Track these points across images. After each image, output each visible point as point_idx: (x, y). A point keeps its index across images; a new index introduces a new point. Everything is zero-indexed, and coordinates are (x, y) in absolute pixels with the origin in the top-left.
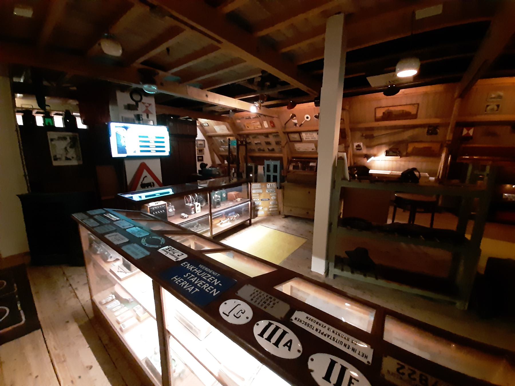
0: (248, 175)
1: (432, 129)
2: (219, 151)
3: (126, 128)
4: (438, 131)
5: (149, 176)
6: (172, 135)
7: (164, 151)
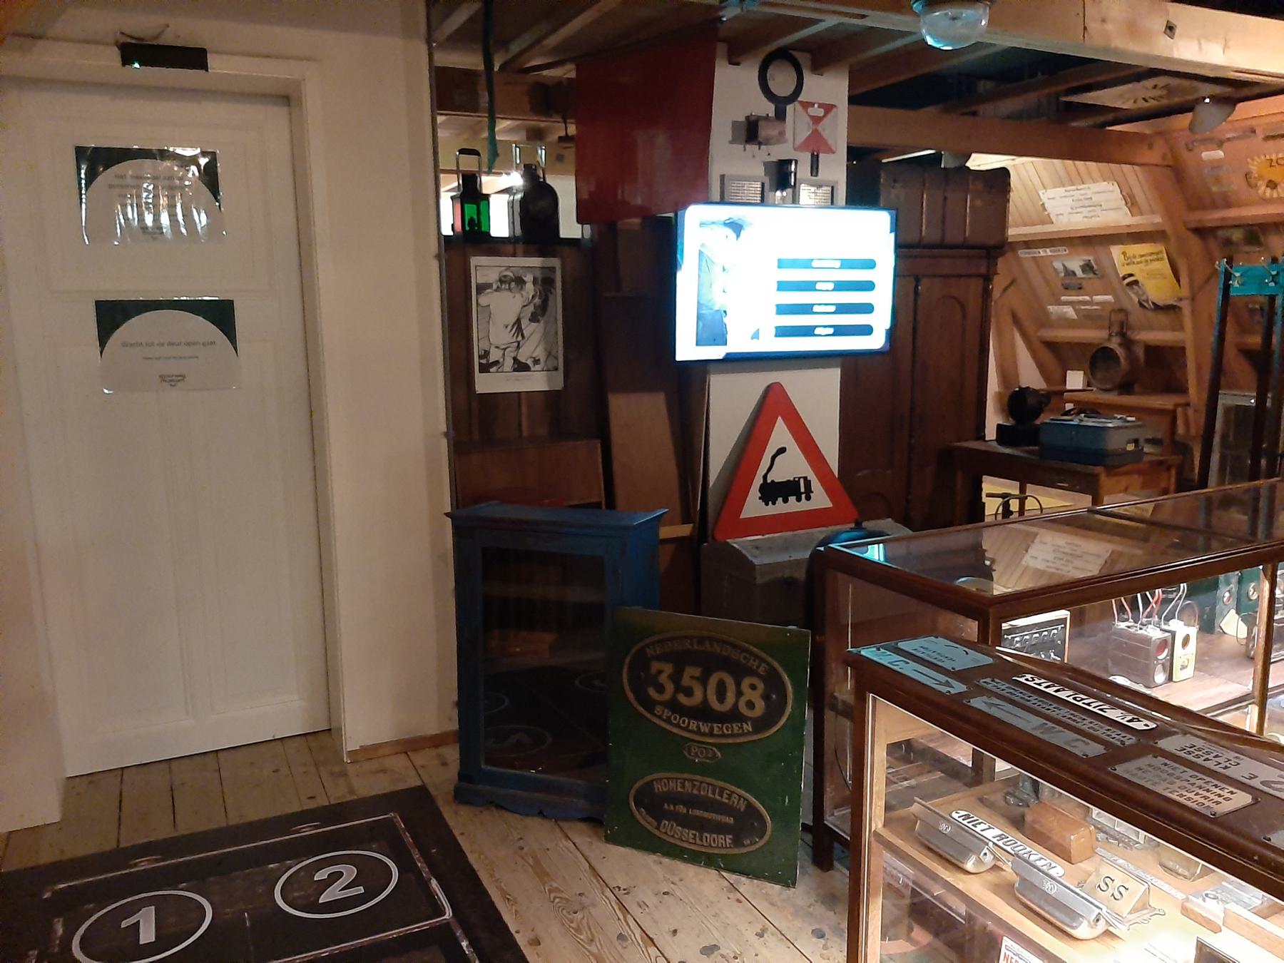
0: (1256, 462)
2: (1045, 321)
3: (736, 227)
5: (794, 449)
7: (866, 330)
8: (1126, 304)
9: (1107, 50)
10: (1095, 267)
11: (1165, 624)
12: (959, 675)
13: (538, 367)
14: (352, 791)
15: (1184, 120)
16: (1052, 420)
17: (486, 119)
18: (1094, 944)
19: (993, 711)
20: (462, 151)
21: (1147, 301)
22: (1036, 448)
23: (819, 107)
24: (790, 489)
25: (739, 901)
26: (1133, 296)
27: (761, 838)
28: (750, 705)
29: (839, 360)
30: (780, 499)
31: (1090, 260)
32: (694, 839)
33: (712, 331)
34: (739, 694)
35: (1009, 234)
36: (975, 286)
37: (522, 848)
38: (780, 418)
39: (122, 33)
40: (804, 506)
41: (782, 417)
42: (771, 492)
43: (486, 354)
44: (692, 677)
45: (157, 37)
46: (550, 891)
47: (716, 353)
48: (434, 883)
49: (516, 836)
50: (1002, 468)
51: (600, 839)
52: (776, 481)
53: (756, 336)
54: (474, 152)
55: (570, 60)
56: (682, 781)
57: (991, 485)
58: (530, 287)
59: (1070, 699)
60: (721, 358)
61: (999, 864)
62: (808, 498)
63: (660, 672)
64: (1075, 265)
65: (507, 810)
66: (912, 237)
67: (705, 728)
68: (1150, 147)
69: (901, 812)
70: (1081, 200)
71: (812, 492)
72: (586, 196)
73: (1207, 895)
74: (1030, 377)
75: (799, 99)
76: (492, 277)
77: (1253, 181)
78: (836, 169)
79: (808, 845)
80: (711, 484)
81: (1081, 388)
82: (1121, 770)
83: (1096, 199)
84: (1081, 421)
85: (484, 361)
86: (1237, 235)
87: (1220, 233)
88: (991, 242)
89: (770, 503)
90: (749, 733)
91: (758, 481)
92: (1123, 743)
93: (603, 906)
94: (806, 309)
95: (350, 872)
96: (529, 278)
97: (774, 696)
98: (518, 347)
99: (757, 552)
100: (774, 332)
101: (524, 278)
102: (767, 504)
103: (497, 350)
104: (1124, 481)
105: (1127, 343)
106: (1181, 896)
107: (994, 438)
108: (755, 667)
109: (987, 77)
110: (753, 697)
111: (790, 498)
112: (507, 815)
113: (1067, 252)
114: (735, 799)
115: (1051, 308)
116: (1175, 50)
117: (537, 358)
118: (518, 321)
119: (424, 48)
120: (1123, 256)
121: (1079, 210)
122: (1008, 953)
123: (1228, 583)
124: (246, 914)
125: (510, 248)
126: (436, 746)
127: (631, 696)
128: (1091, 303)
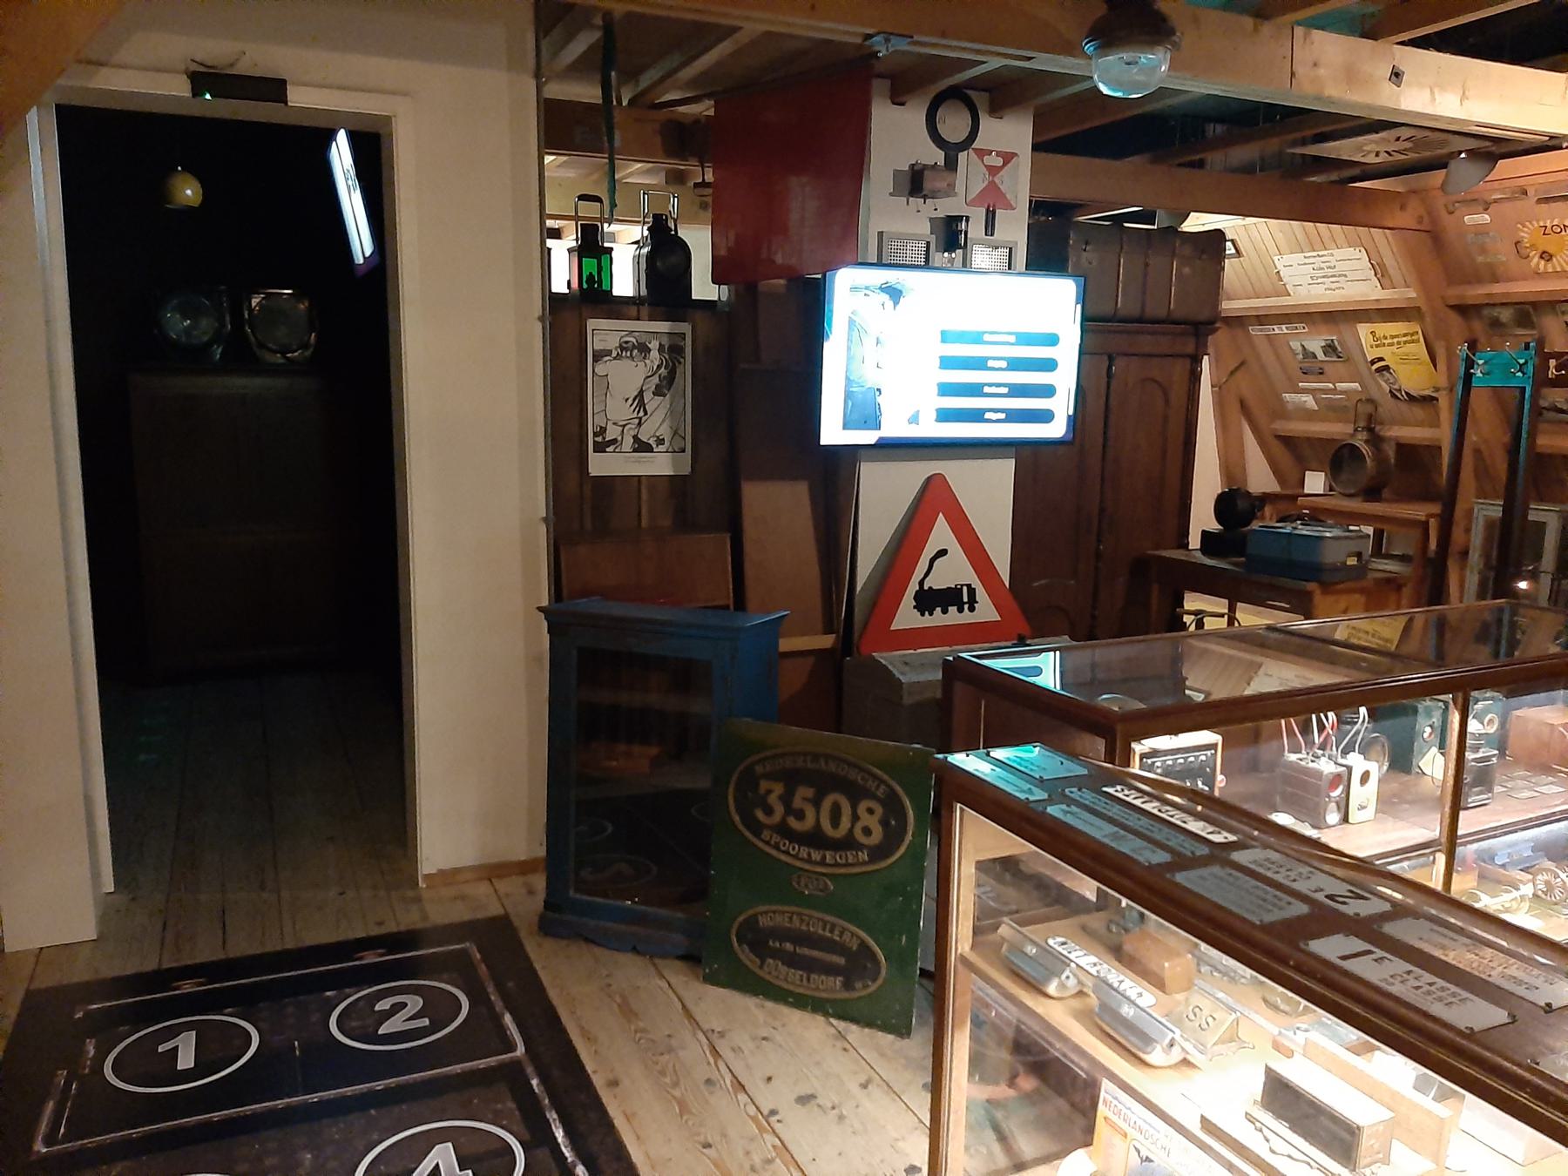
2: (1281, 412)
3: (894, 293)
6: (1091, 322)
7: (1045, 416)
8: (1375, 395)
9: (1318, 98)
10: (1339, 349)
11: (1342, 757)
12: (1041, 783)
13: (661, 448)
14: (425, 917)
15: (1438, 177)
16: (1261, 527)
17: (607, 161)
18: (1169, 1072)
19: (1069, 819)
20: (582, 198)
21: (1400, 390)
22: (1243, 559)
23: (997, 155)
24: (951, 597)
25: (845, 1050)
26: (1383, 384)
27: (874, 980)
28: (867, 831)
30: (939, 609)
31: (1332, 340)
32: (802, 980)
33: (863, 412)
34: (855, 818)
35: (1223, 307)
36: (1180, 369)
37: (610, 985)
38: (941, 515)
39: (193, 61)
40: (967, 617)
42: (928, 600)
43: (603, 430)
44: (805, 799)
45: (232, 65)
46: (636, 1032)
47: (868, 437)
48: (508, 1019)
49: (605, 972)
50: (1208, 583)
51: (698, 978)
52: (934, 588)
53: (914, 420)
54: (597, 199)
55: (708, 96)
56: (790, 915)
57: (1193, 602)
58: (655, 354)
59: (1155, 811)
60: (873, 443)
61: (1085, 990)
62: (972, 609)
63: (769, 792)
64: (1316, 345)
65: (599, 945)
66: (1106, 309)
67: (816, 856)
68: (1403, 208)
69: (991, 937)
70: (1323, 269)
71: (977, 602)
72: (723, 252)
73: (1298, 1028)
74: (1260, 479)
75: (973, 146)
76: (612, 342)
77: (1523, 252)
78: (1015, 228)
79: (930, 992)
80: (859, 588)
81: (1322, 492)
82: (1180, 878)
83: (1341, 267)
84: (1295, 528)
85: (599, 439)
86: (1505, 315)
87: (1486, 312)
88: (1204, 315)
89: (927, 613)
90: (864, 863)
91: (913, 587)
92: (1193, 853)
93: (692, 1050)
94: (975, 390)
95: (415, 1003)
96: (654, 345)
97: (893, 823)
98: (640, 424)
99: (907, 669)
100: (934, 416)
101: (649, 346)
102: (923, 615)
103: (614, 426)
104: (1343, 601)
105: (1375, 440)
106: (1275, 1031)
107: (1199, 547)
108: (873, 789)
109: (1220, 120)
110: (870, 822)
111: (950, 608)
112: (598, 951)
113: (1307, 330)
114: (847, 937)
115: (1287, 396)
116: (1402, 99)
117: (661, 437)
118: (641, 393)
119: (532, 83)
120: (1371, 337)
121: (1319, 281)
122: (1108, 1096)
123: (1429, 714)
124: (296, 1043)
125: (633, 310)
126: (523, 873)
127: (737, 818)
128: (1334, 391)
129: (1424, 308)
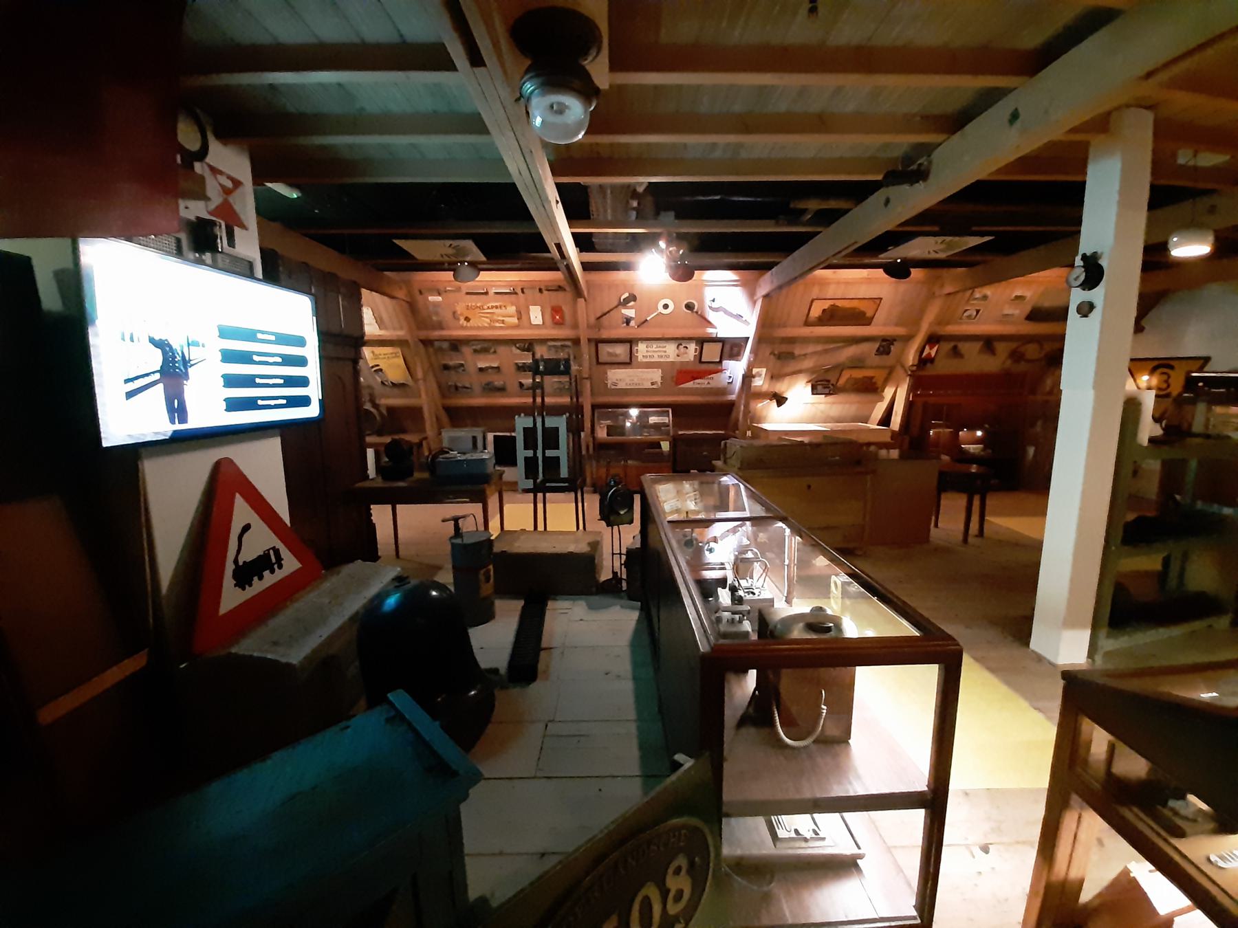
1: (886, 345)
4: (892, 349)
5: (258, 525)
7: (304, 401)
24: (264, 563)
29: (277, 431)
30: (256, 578)
38: (238, 495)
40: (280, 574)
41: (240, 494)
42: (245, 574)
62: (280, 567)
89: (247, 586)
91: (230, 567)
102: (244, 589)
129: (410, 341)
